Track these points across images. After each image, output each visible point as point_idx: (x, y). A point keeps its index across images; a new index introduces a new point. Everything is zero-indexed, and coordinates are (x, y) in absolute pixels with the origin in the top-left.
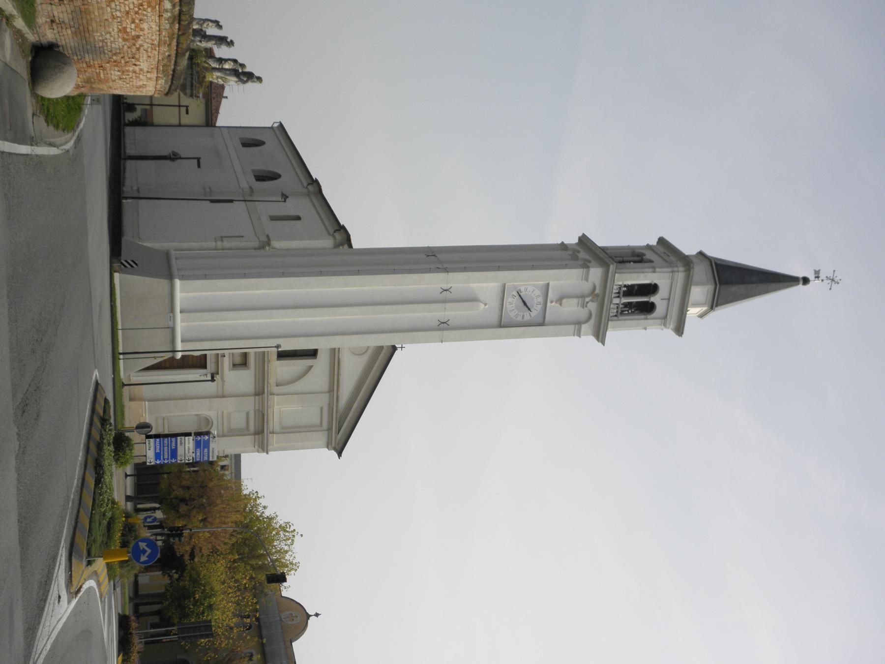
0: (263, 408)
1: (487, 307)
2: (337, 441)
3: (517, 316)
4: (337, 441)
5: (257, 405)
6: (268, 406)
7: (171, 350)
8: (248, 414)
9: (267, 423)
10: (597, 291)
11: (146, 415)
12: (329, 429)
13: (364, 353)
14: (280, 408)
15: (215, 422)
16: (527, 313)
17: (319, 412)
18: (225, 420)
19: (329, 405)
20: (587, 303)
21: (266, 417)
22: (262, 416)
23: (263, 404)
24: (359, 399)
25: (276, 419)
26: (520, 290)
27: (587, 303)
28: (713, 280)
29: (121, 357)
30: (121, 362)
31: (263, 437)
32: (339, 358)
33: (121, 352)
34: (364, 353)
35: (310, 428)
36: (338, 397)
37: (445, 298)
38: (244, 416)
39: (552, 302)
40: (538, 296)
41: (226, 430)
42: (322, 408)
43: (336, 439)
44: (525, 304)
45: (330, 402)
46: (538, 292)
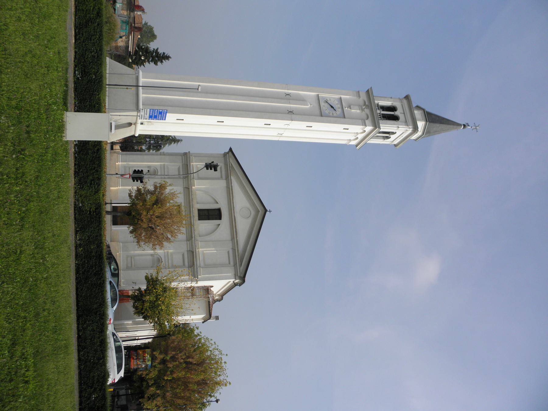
0: (192, 248)
1: (312, 106)
2: (241, 272)
3: (329, 113)
4: (241, 272)
5: (189, 247)
6: (195, 245)
7: (136, 85)
8: (183, 255)
9: (196, 257)
10: (367, 104)
11: (120, 252)
12: (235, 265)
13: (250, 216)
14: (203, 251)
15: (163, 260)
16: (334, 112)
17: (227, 255)
18: (170, 257)
19: (232, 249)
20: (364, 109)
21: (194, 253)
22: (192, 253)
23: (192, 245)
24: (250, 243)
25: (201, 258)
26: (327, 100)
27: (364, 109)
28: (425, 118)
29: (107, 86)
30: (107, 89)
31: (194, 268)
32: (234, 216)
33: (108, 83)
34: (250, 216)
35: (223, 265)
36: (237, 242)
37: (288, 97)
38: (181, 256)
39: (345, 108)
40: (337, 104)
41: (170, 265)
42: (228, 252)
43: (240, 271)
44: (332, 107)
45: (233, 247)
46: (337, 102)
